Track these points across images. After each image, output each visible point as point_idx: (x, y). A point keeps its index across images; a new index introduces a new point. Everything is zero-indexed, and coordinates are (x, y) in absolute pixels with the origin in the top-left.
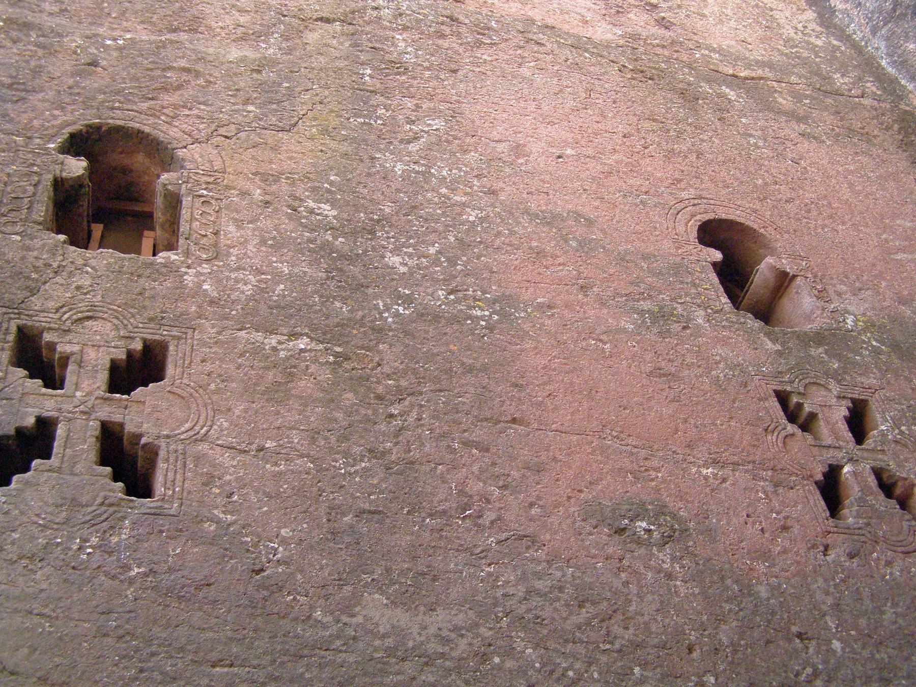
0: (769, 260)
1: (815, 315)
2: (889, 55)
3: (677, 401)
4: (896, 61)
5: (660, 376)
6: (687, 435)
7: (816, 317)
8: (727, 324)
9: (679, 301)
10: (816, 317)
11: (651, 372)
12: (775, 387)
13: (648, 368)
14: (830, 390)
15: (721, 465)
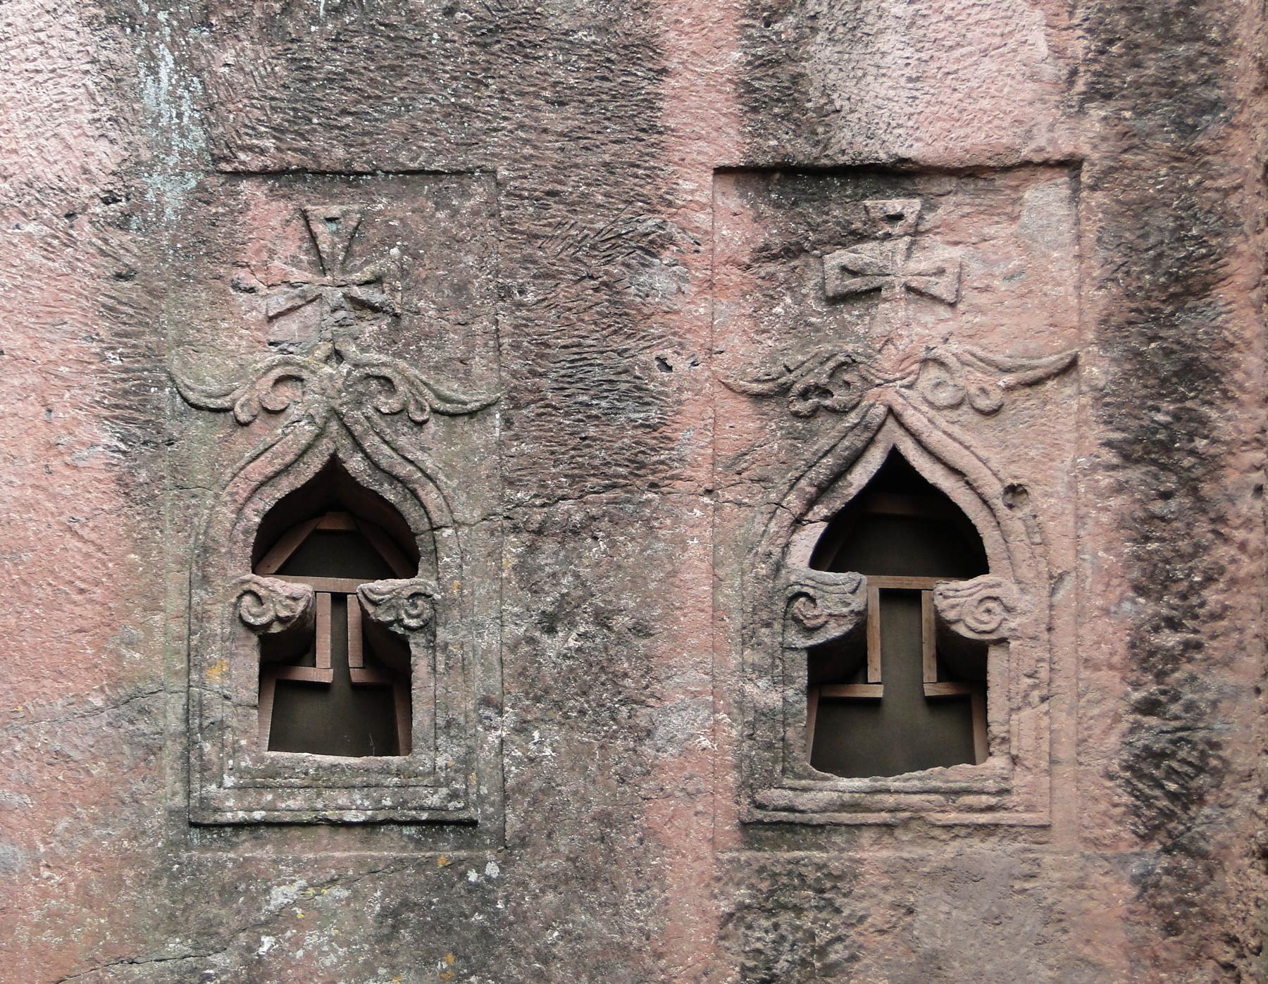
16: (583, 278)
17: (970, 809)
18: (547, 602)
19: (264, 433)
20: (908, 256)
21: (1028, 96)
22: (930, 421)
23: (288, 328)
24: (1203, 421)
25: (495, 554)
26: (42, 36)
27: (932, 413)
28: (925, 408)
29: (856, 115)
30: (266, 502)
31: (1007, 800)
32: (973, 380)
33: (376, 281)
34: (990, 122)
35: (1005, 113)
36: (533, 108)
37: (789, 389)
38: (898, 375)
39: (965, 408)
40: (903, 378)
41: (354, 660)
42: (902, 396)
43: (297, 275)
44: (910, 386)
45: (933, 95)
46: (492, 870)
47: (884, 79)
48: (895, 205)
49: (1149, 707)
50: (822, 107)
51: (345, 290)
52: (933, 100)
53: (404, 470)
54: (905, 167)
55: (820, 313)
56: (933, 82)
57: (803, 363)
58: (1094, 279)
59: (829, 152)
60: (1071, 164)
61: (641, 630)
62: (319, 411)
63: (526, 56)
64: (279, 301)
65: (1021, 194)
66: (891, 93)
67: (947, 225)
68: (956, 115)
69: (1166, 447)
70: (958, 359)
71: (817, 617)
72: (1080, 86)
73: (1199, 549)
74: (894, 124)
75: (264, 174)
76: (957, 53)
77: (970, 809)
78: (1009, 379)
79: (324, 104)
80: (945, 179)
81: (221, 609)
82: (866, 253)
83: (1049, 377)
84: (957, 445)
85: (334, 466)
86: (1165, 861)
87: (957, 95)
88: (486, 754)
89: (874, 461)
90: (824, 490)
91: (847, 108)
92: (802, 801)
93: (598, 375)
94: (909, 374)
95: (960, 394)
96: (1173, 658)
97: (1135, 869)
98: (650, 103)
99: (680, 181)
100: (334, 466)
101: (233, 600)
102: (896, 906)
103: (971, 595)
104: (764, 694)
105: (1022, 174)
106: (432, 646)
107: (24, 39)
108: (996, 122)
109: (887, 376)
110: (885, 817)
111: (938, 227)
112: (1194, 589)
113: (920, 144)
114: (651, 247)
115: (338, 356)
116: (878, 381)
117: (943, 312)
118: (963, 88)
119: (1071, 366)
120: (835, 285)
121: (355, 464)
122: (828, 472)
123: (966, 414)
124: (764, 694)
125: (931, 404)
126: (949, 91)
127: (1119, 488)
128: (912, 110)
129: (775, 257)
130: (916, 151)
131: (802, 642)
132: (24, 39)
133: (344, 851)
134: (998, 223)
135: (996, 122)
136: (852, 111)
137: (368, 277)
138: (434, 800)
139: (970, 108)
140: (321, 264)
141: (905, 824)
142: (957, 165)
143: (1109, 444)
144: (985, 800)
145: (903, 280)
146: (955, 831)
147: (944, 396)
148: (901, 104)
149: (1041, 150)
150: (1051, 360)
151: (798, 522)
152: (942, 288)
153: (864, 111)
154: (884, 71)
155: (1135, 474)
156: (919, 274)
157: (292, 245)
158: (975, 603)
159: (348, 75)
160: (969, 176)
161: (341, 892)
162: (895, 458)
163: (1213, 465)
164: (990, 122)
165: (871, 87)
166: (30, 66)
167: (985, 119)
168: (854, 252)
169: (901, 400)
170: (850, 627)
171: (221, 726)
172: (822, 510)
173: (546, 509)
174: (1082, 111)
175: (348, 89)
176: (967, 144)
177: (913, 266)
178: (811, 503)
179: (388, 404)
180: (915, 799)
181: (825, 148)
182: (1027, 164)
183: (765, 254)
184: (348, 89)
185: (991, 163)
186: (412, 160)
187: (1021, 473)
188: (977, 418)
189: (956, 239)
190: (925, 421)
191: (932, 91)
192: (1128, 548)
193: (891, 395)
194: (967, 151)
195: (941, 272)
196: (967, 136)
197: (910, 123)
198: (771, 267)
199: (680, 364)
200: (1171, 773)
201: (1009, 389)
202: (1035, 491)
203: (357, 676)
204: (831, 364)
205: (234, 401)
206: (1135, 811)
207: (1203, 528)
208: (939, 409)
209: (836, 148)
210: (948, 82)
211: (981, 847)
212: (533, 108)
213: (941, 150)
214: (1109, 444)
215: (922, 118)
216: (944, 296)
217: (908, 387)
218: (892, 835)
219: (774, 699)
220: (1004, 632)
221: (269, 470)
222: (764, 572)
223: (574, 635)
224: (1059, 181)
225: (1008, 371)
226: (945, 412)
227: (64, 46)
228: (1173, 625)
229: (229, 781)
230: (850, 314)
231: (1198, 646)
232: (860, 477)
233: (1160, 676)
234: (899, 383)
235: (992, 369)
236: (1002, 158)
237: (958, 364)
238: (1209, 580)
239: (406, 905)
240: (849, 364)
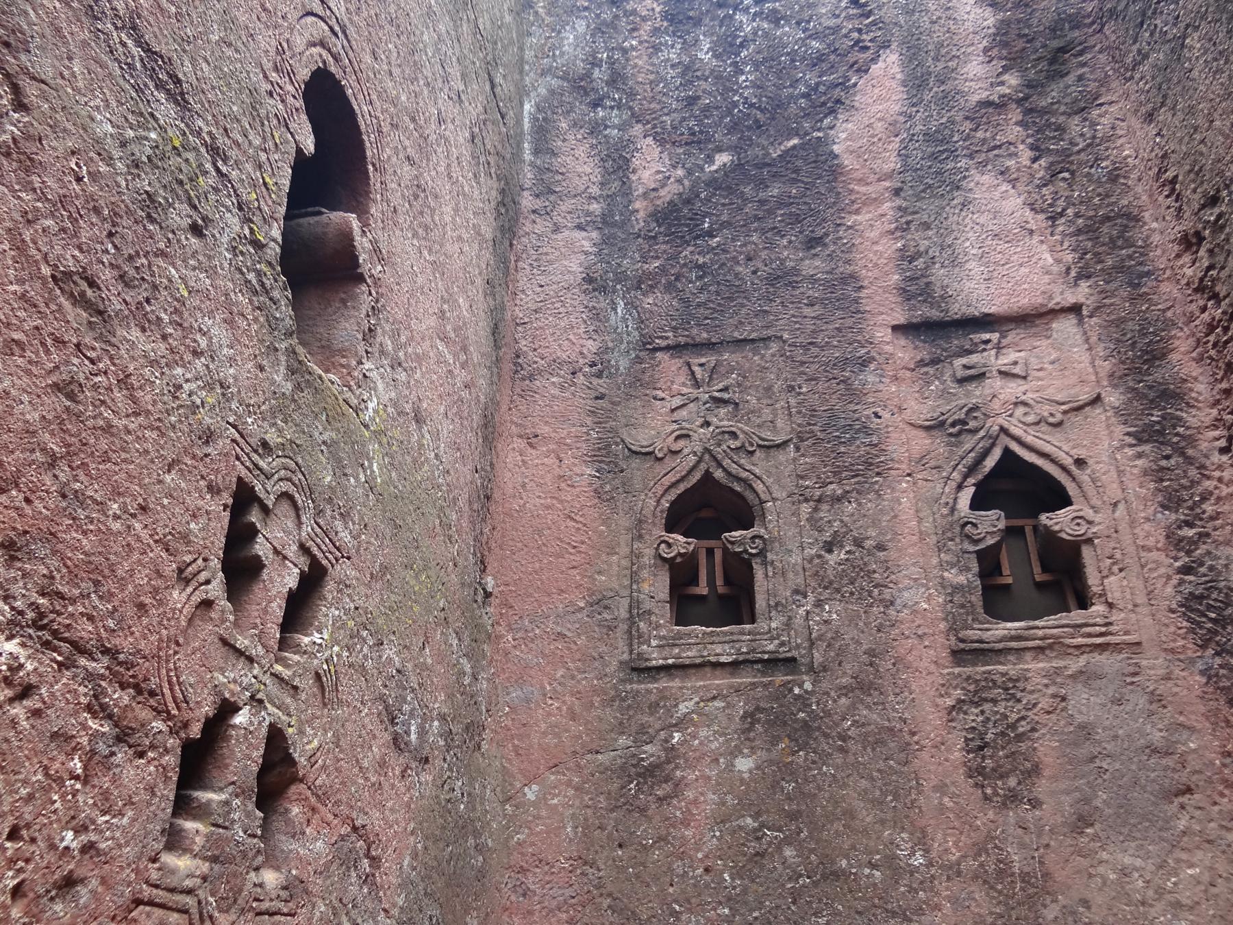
0: (352, 217)
1: (343, 361)
2: (539, 108)
3: (71, 396)
4: (538, 120)
5: (80, 301)
6: (28, 510)
7: (343, 366)
8: (254, 281)
9: (220, 163)
10: (343, 366)
11: (68, 275)
12: (244, 472)
13: (70, 259)
14: (299, 524)
15: (47, 636)
18: (827, 536)
19: (670, 462)
23: (684, 413)
24: (1180, 419)
25: (796, 514)
30: (672, 496)
32: (1045, 410)
33: (725, 389)
41: (719, 582)
43: (685, 390)
46: (808, 686)
48: (987, 336)
49: (1186, 570)
53: (744, 475)
60: (1075, 309)
61: (881, 547)
62: (698, 449)
64: (677, 401)
69: (1161, 433)
72: (1073, 274)
73: (1193, 483)
75: (668, 348)
76: (1007, 266)
81: (649, 552)
82: (974, 358)
85: (708, 475)
86: (1218, 660)
88: (798, 621)
90: (972, 470)
92: (986, 635)
93: (843, 422)
96: (1194, 542)
97: (1200, 665)
98: (856, 301)
100: (708, 475)
104: (954, 577)
106: (765, 563)
112: (1196, 505)
114: (864, 363)
115: (707, 424)
119: (1097, 400)
120: (961, 373)
121: (718, 474)
123: (1044, 427)
124: (954, 577)
127: (1139, 456)
130: (993, 308)
131: (972, 548)
133: (721, 681)
138: (771, 647)
140: (697, 384)
141: (1050, 647)
143: (1128, 434)
146: (1083, 649)
147: (1031, 419)
151: (960, 487)
152: (1017, 370)
155: (1147, 448)
157: (683, 377)
161: (719, 704)
162: (1007, 452)
163: (1191, 441)
171: (650, 613)
172: (971, 481)
178: (966, 477)
179: (734, 444)
183: (921, 363)
187: (1082, 453)
192: (1152, 485)
193: (1000, 420)
199: (886, 415)
200: (1209, 607)
202: (1090, 462)
203: (721, 590)
206: (1193, 631)
207: (1193, 472)
211: (1098, 658)
214: (1128, 434)
218: (1044, 653)
219: (962, 579)
225: (1063, 404)
228: (1190, 525)
229: (654, 643)
231: (1208, 535)
232: (990, 463)
233: (1188, 553)
238: (1204, 499)
239: (758, 709)
240: (975, 408)
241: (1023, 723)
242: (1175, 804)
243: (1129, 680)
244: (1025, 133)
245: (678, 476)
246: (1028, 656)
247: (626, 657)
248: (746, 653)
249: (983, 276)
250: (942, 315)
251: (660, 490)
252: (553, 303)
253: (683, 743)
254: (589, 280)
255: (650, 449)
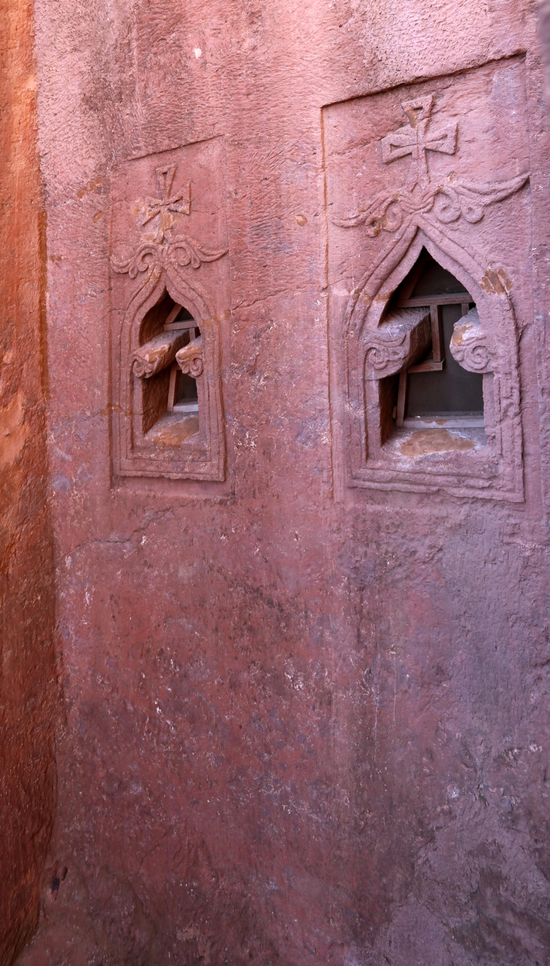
16: (262, 180)
17: (472, 487)
20: (425, 132)
21: (489, 22)
22: (441, 232)
26: (69, 123)
27: (442, 227)
28: (438, 225)
29: (390, 60)
30: (141, 315)
31: (495, 483)
34: (466, 43)
35: (475, 36)
36: (238, 100)
37: (365, 222)
38: (421, 206)
39: (461, 220)
40: (424, 207)
42: (424, 218)
44: (429, 211)
45: (432, 37)
47: (404, 36)
50: (372, 61)
51: (168, 206)
52: (433, 39)
54: (421, 79)
55: (381, 172)
56: (431, 29)
57: (371, 205)
58: (537, 126)
59: (378, 84)
60: (519, 55)
63: (234, 76)
65: (491, 78)
66: (409, 42)
67: (449, 105)
68: (446, 45)
70: (455, 191)
71: (382, 362)
74: (411, 59)
76: (444, 10)
77: (472, 487)
78: (487, 200)
79: (160, 122)
80: (447, 79)
83: (512, 194)
84: (455, 246)
87: (446, 33)
89: (414, 255)
91: (384, 58)
94: (428, 204)
95: (458, 213)
99: (304, 119)
101: (130, 365)
102: (431, 547)
103: (468, 345)
105: (490, 67)
107: (64, 126)
108: (471, 42)
109: (416, 207)
110: (423, 488)
111: (445, 107)
113: (427, 67)
116: (411, 211)
117: (447, 158)
118: (449, 28)
120: (388, 155)
122: (385, 270)
125: (442, 222)
126: (441, 32)
128: (421, 49)
129: (357, 145)
130: (424, 71)
132: (64, 126)
134: (479, 97)
135: (471, 42)
136: (387, 59)
137: (176, 199)
139: (454, 39)
142: (449, 72)
144: (481, 483)
145: (424, 146)
146: (465, 500)
147: (449, 215)
148: (414, 47)
149: (499, 51)
150: (515, 183)
153: (394, 57)
154: (403, 32)
156: (432, 141)
158: (471, 350)
159: (168, 106)
160: (460, 74)
162: (424, 252)
164: (466, 43)
165: (397, 43)
166: (66, 136)
167: (464, 42)
168: (398, 133)
169: (423, 222)
170: (401, 366)
173: (249, 307)
174: (523, 21)
175: (168, 112)
176: (453, 60)
177: (431, 135)
180: (440, 479)
181: (376, 82)
182: (490, 62)
184: (168, 112)
185: (471, 66)
186: (192, 138)
188: (469, 226)
189: (454, 113)
190: (438, 233)
191: (431, 35)
194: (455, 64)
195: (445, 137)
196: (453, 55)
197: (421, 56)
198: (355, 151)
201: (487, 206)
204: (386, 204)
205: (129, 269)
208: (446, 223)
209: (381, 81)
210: (440, 27)
211: (482, 511)
212: (238, 100)
213: (439, 67)
215: (426, 52)
216: (447, 151)
217: (427, 212)
218: (429, 498)
220: (490, 369)
221: (141, 301)
222: (353, 336)
223: (262, 378)
224: (514, 66)
225: (486, 194)
226: (450, 225)
227: (76, 124)
230: (396, 169)
234: (422, 210)
235: (476, 195)
236: (477, 62)
237: (455, 195)
241: (400, 570)
242: (533, 674)
243: (506, 539)
244: (71, 586)
245: (144, 297)
246: (414, 499)
247: (426, 499)
248: (188, 473)
249: (416, 28)
250: (371, 86)
251: (132, 310)
252: (64, 129)
253: (147, 545)
254: (87, 100)
255: (125, 270)
